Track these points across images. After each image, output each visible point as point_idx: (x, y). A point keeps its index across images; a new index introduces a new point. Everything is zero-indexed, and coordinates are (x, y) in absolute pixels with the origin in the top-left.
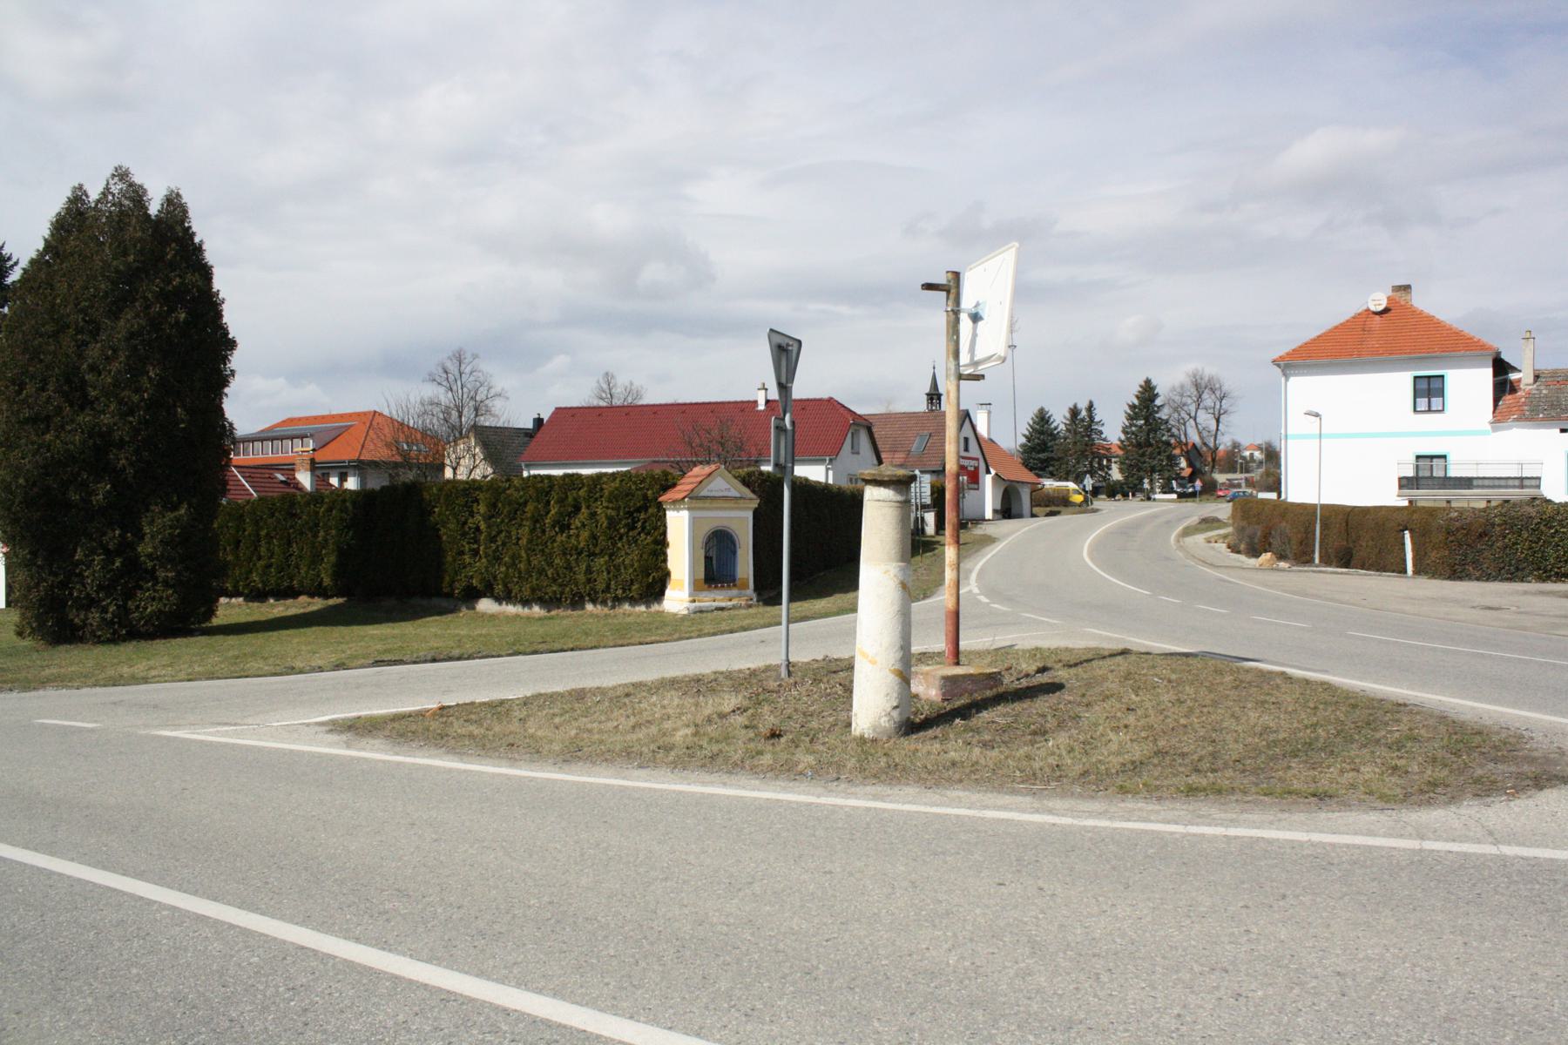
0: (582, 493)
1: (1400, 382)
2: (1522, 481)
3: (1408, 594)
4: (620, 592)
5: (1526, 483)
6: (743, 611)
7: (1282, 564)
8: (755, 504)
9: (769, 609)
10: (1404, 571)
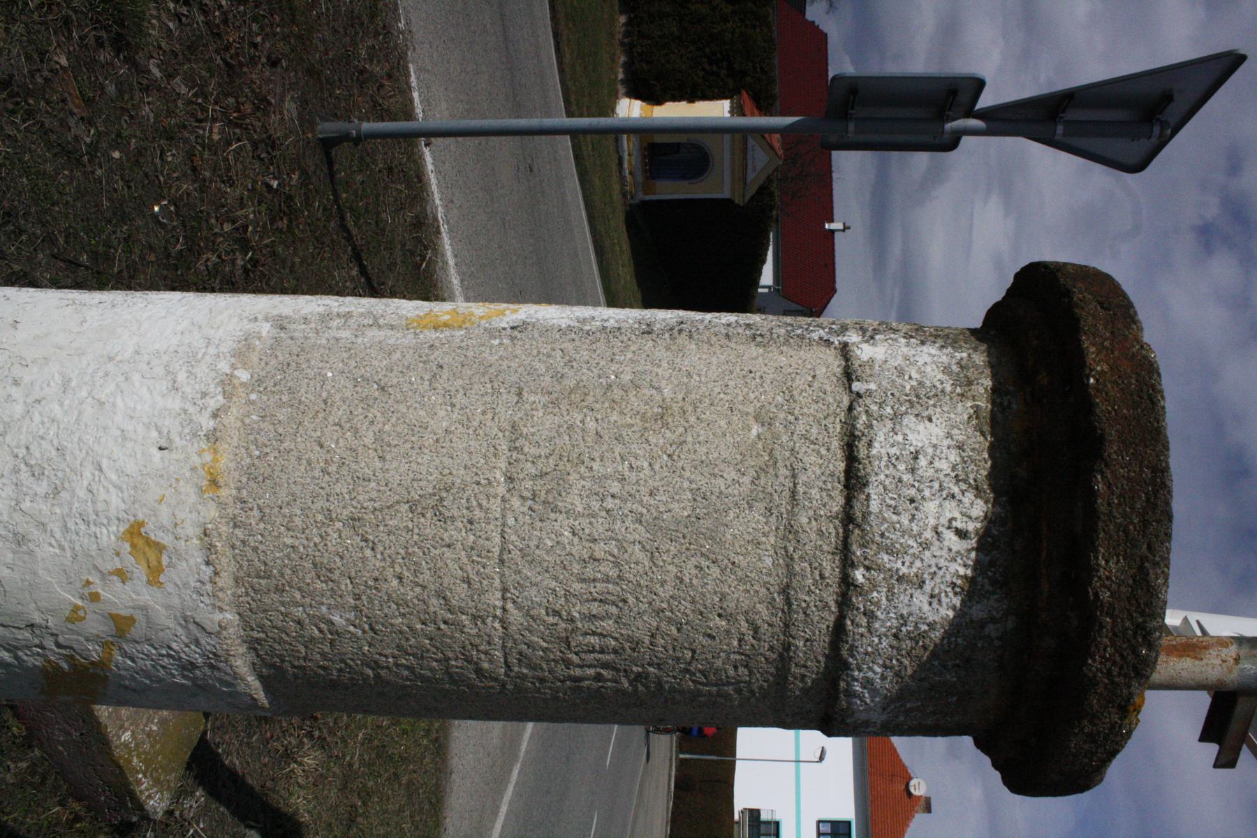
6: (617, 187)
8: (738, 201)
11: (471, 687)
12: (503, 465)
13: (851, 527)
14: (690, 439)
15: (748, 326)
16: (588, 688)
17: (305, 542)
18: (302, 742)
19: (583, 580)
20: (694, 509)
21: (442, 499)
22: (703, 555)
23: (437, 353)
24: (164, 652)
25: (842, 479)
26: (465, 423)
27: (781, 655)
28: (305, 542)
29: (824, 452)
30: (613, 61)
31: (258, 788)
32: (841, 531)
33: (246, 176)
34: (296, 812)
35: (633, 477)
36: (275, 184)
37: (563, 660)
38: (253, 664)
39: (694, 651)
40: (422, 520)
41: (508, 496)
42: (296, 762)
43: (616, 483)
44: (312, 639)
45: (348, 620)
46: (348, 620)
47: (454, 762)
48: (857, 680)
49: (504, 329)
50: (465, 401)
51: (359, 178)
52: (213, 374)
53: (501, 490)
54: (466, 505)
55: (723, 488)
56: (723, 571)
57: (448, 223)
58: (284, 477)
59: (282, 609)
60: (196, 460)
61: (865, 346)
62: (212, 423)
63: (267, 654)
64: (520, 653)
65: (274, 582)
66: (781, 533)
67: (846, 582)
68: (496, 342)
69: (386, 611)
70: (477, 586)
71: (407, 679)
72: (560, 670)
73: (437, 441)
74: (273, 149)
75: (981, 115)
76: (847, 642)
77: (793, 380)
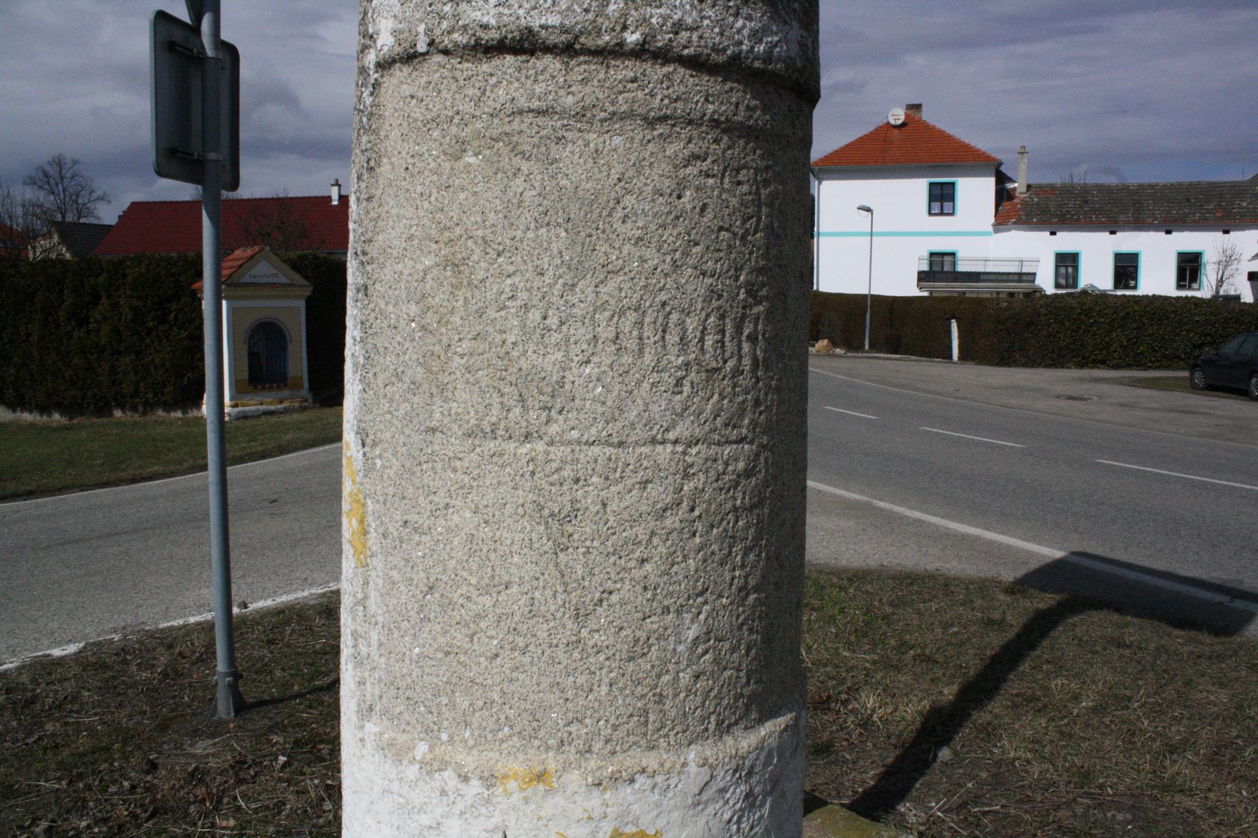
0: (101, 279)
1: (918, 188)
2: (1019, 276)
3: (954, 377)
4: (150, 396)
5: (1024, 278)
6: (295, 416)
7: (838, 351)
8: (308, 292)
9: (327, 410)
10: (950, 357)
11: (766, 484)
12: (512, 446)
13: (577, 46)
14: (480, 233)
15: (359, 178)
16: (765, 351)
17: (605, 670)
18: (852, 711)
19: (641, 351)
20: (559, 225)
21: (552, 515)
22: (610, 215)
23: (391, 529)
24: (735, 827)
25: (524, 57)
26: (466, 490)
27: (725, 131)
28: (605, 670)
29: (493, 80)
30: (162, 422)
31: (898, 752)
32: (582, 58)
33: (274, 789)
34: (920, 713)
35: (523, 295)
36: (282, 759)
37: (733, 377)
38: (746, 728)
39: (721, 229)
40: (576, 536)
41: (546, 439)
42: (871, 716)
43: (530, 315)
44: (716, 661)
45: (692, 621)
46: (692, 621)
47: (872, 563)
48: (752, 48)
49: (365, 454)
50: (442, 493)
51: (278, 673)
52: (421, 783)
53: (540, 446)
54: (558, 487)
55: (534, 193)
56: (629, 192)
57: (328, 582)
58: (532, 697)
59: (682, 695)
60: (516, 798)
61: (379, 43)
62: (475, 782)
63: (734, 713)
64: (727, 425)
65: (651, 705)
66: (586, 127)
67: (641, 52)
68: (379, 462)
69: (680, 577)
70: (649, 472)
71: (759, 555)
72: (745, 381)
73: (486, 522)
74: (245, 762)
75: (198, 19)
76: (709, 55)
77: (415, 120)
